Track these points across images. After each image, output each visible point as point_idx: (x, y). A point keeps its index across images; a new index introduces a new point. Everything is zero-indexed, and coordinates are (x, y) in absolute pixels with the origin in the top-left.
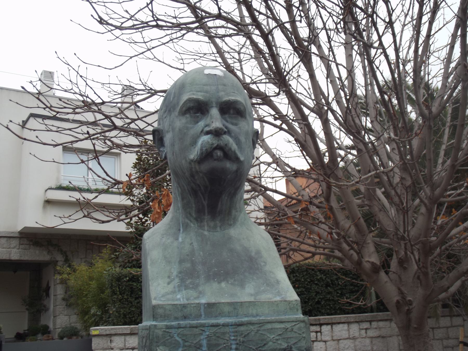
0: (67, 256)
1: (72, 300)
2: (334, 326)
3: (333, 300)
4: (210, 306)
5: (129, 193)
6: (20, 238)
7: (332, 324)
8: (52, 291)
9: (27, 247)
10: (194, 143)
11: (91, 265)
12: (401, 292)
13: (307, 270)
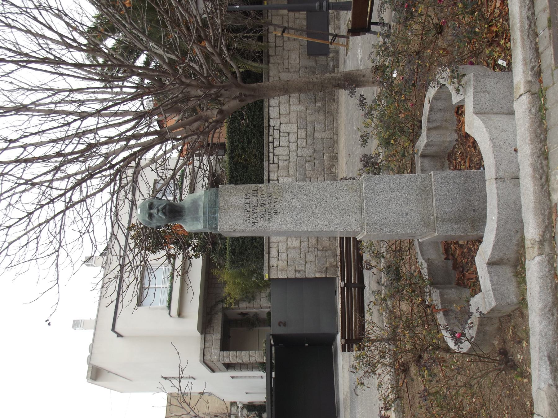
0: (219, 301)
1: (250, 295)
2: (271, 117)
3: (253, 116)
4: (204, 214)
5: (174, 257)
6: (205, 334)
7: (269, 118)
8: (244, 311)
9: (212, 329)
10: (161, 217)
11: (225, 283)
12: (234, 98)
13: (232, 133)
